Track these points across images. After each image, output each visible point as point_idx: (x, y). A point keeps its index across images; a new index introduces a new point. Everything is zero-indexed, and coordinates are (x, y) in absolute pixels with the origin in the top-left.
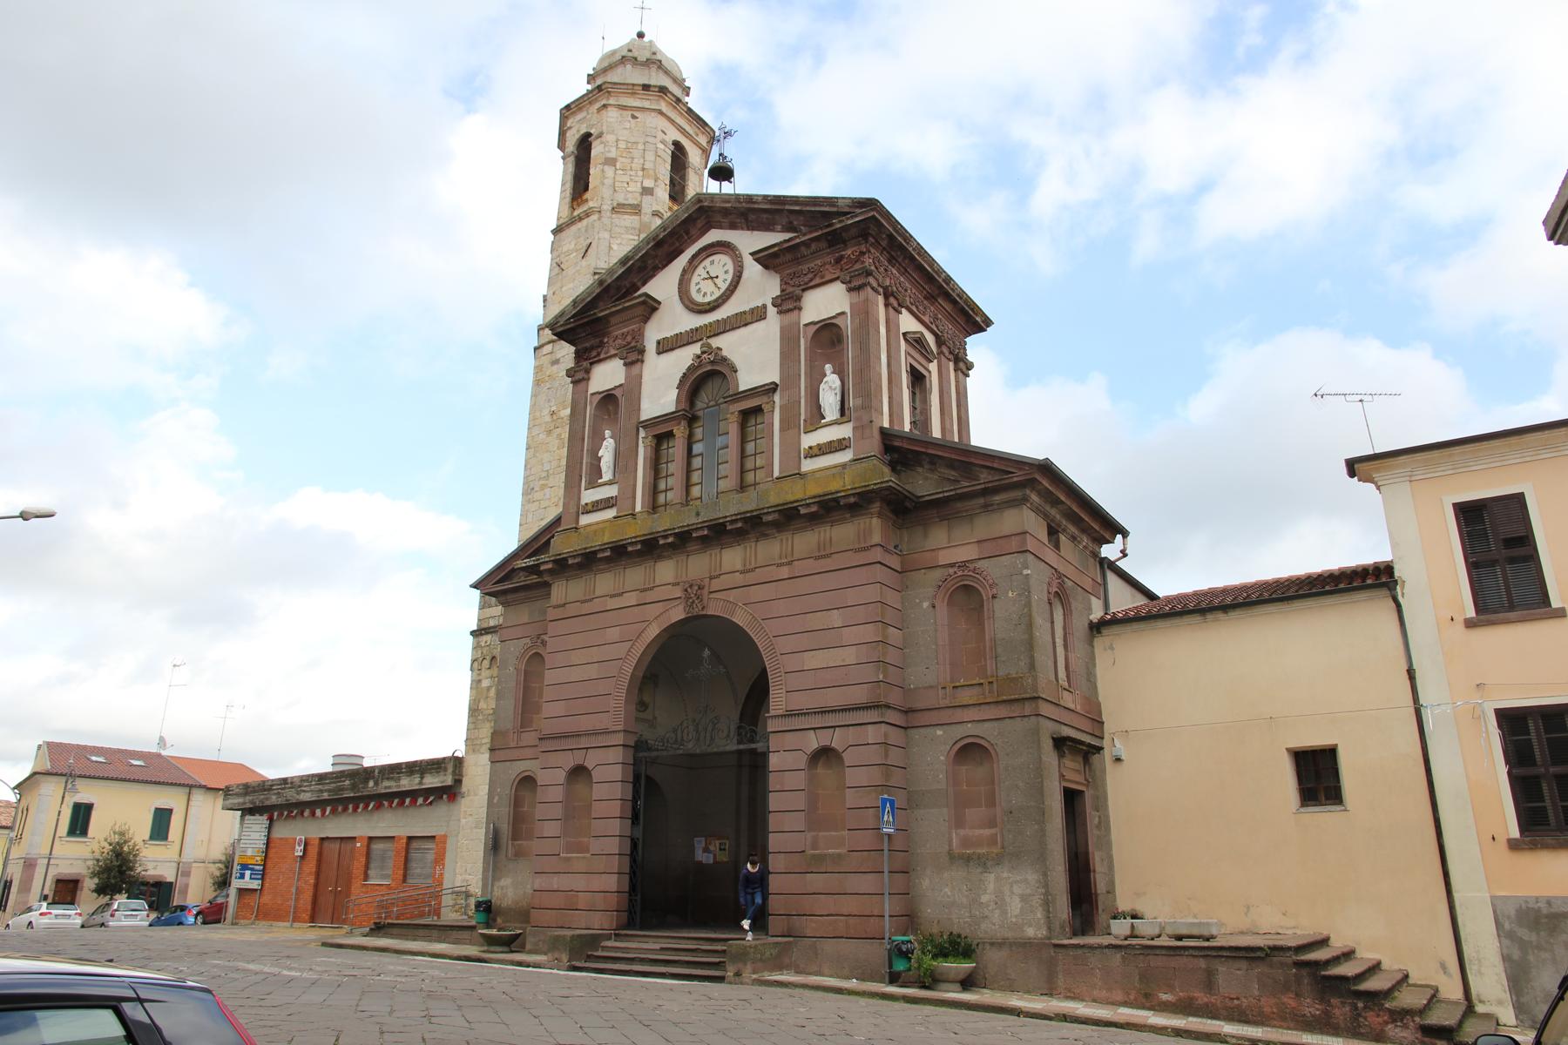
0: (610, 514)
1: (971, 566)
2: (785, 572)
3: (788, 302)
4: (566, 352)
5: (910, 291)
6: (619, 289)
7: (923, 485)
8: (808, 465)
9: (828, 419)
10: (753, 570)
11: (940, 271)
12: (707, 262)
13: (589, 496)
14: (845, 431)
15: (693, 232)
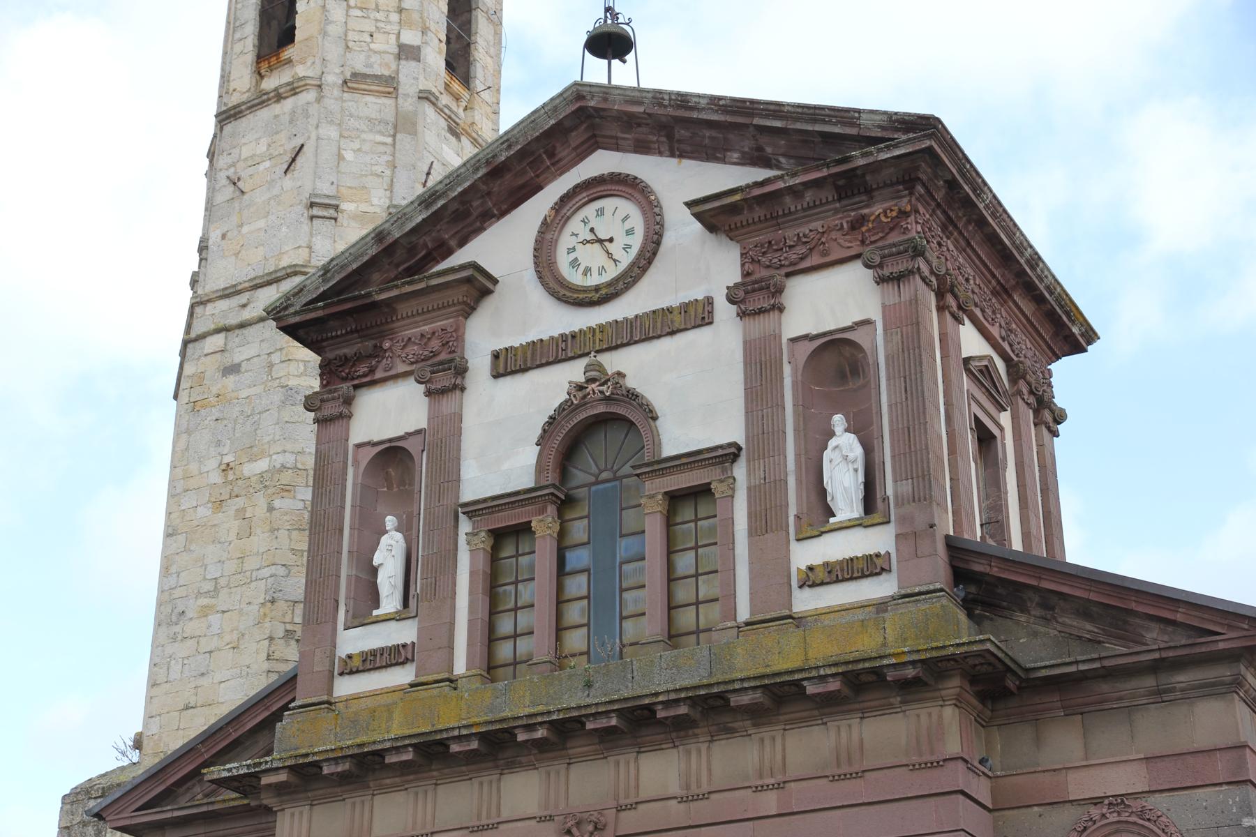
0: (402, 676)
1: (1136, 805)
2: (770, 802)
3: (758, 296)
4: (301, 367)
5: (972, 284)
6: (412, 250)
7: (1031, 645)
9: (842, 515)
10: (703, 797)
11: (1024, 245)
12: (590, 211)
13: (353, 641)
14: (878, 540)
15: (563, 153)
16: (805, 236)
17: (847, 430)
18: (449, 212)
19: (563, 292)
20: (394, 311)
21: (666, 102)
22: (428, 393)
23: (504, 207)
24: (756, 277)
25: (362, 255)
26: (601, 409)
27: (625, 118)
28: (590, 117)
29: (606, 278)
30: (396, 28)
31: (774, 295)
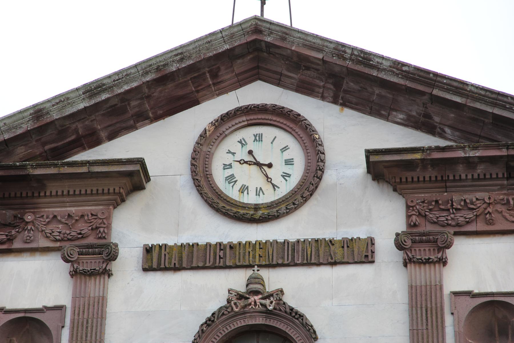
15: (226, 75)
16: (472, 203)
18: (108, 105)
19: (221, 204)
20: (43, 187)
21: (347, 56)
22: (74, 274)
23: (160, 112)
24: (421, 230)
25: (16, 128)
26: (260, 320)
27: (295, 59)
28: (259, 50)
29: (263, 200)
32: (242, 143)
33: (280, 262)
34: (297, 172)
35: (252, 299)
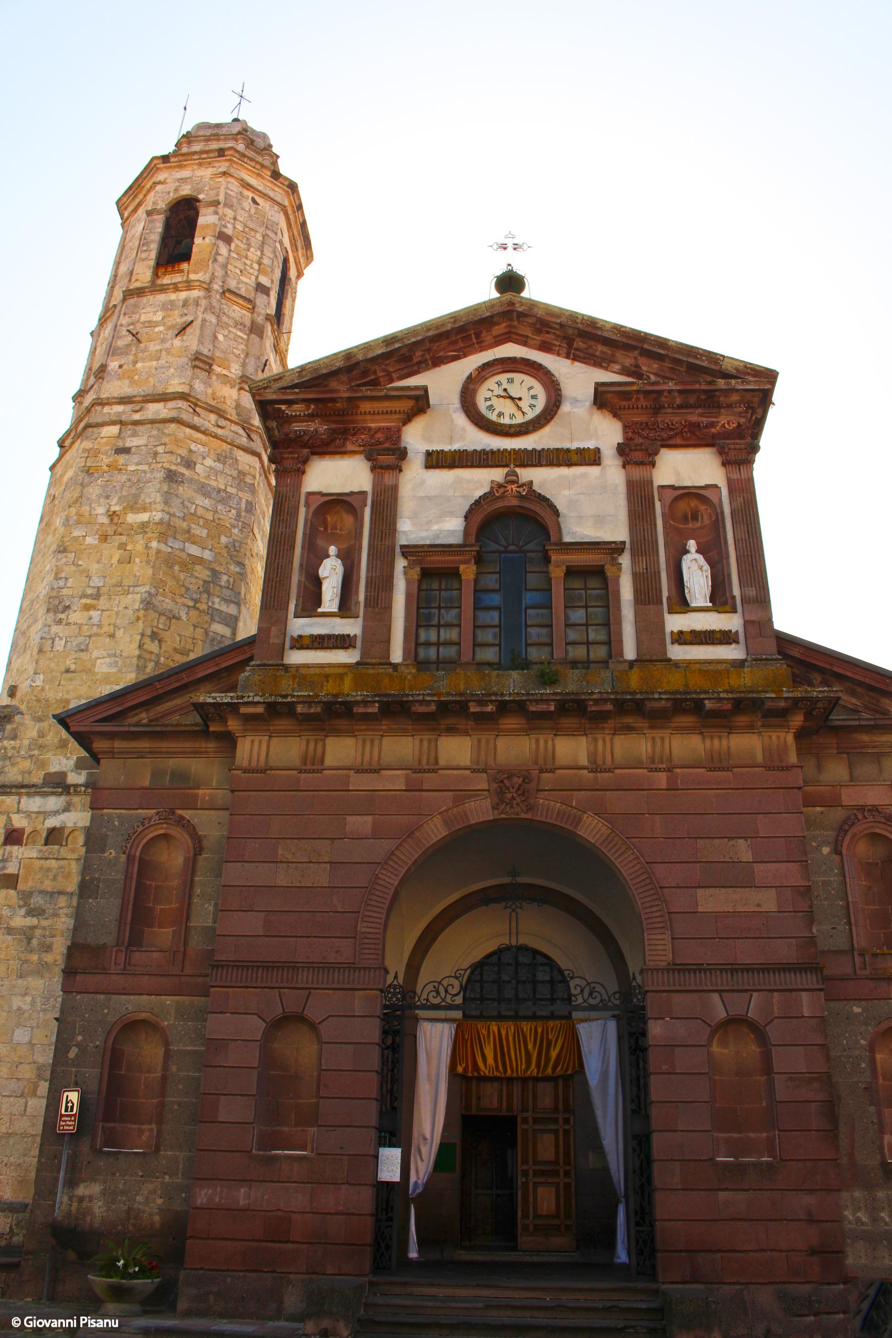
6: (365, 373)
8: (677, 652)
15: (487, 337)
17: (697, 551)
21: (579, 321)
22: (373, 469)
29: (515, 422)
30: (256, 273)
31: (650, 455)
32: (499, 384)
33: (530, 463)
34: (541, 404)
35: (509, 487)
